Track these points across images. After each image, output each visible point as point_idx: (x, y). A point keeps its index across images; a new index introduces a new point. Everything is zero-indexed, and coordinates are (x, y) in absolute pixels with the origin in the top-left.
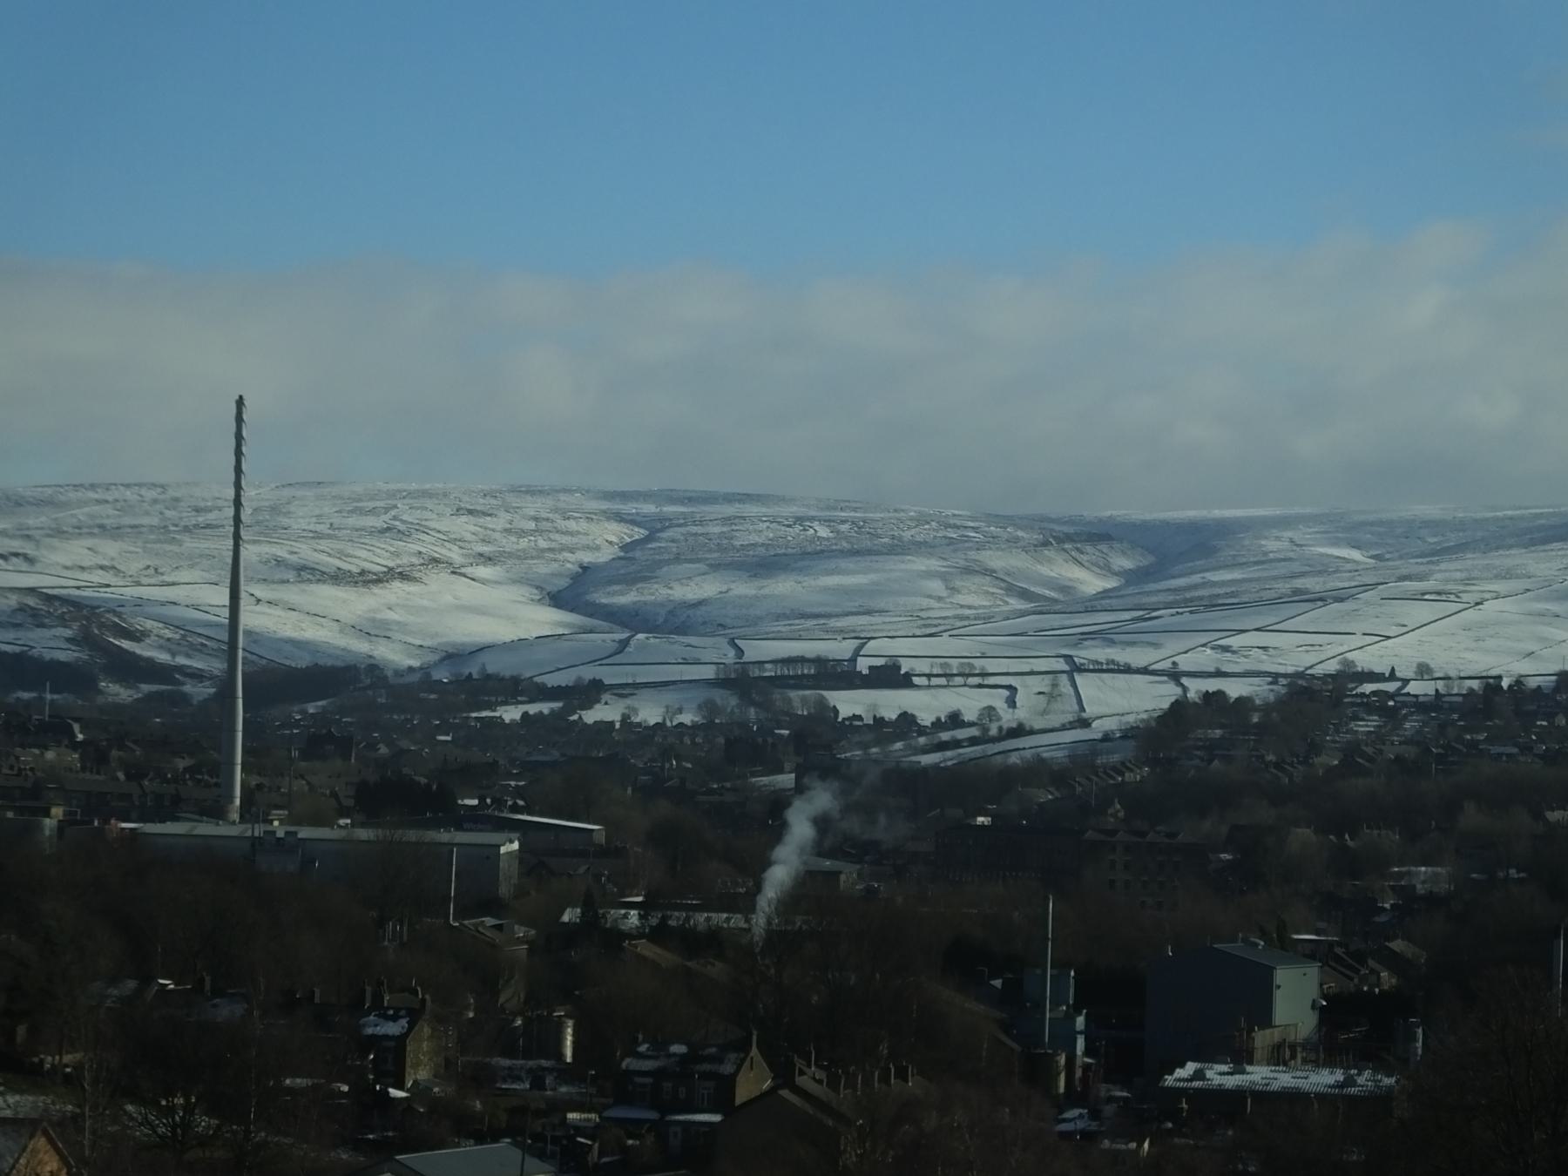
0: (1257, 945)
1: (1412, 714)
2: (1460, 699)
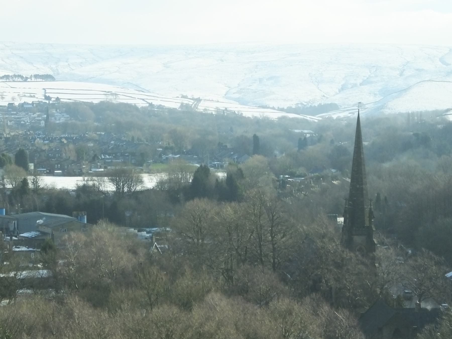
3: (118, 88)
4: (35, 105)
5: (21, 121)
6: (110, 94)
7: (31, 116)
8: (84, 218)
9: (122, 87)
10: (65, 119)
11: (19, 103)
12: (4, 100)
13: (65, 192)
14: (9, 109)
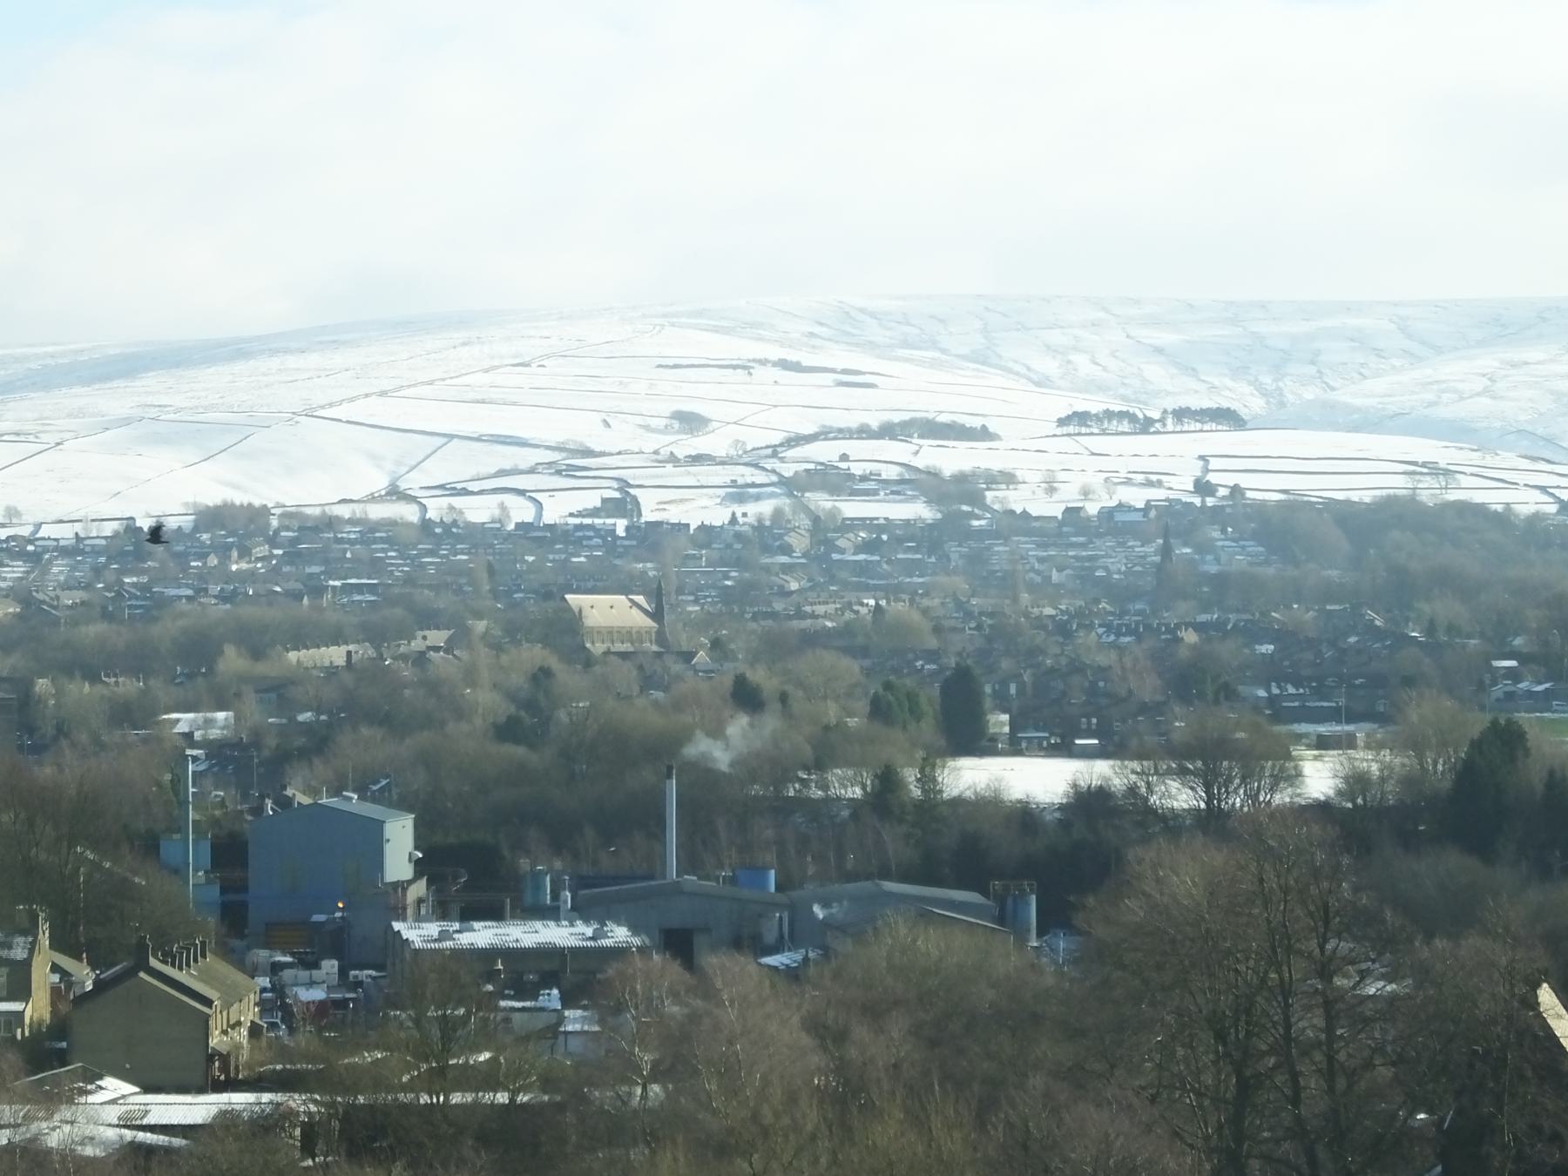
0: (351, 798)
1: (56, 558)
2: (103, 542)
3: (1461, 449)
4: (1153, 514)
5: (1097, 569)
6: (1425, 470)
7: (1134, 551)
8: (1028, 904)
9: (1476, 448)
10: (1249, 558)
11: (1103, 508)
12: (1056, 497)
13: (1025, 816)
14: (1065, 529)
